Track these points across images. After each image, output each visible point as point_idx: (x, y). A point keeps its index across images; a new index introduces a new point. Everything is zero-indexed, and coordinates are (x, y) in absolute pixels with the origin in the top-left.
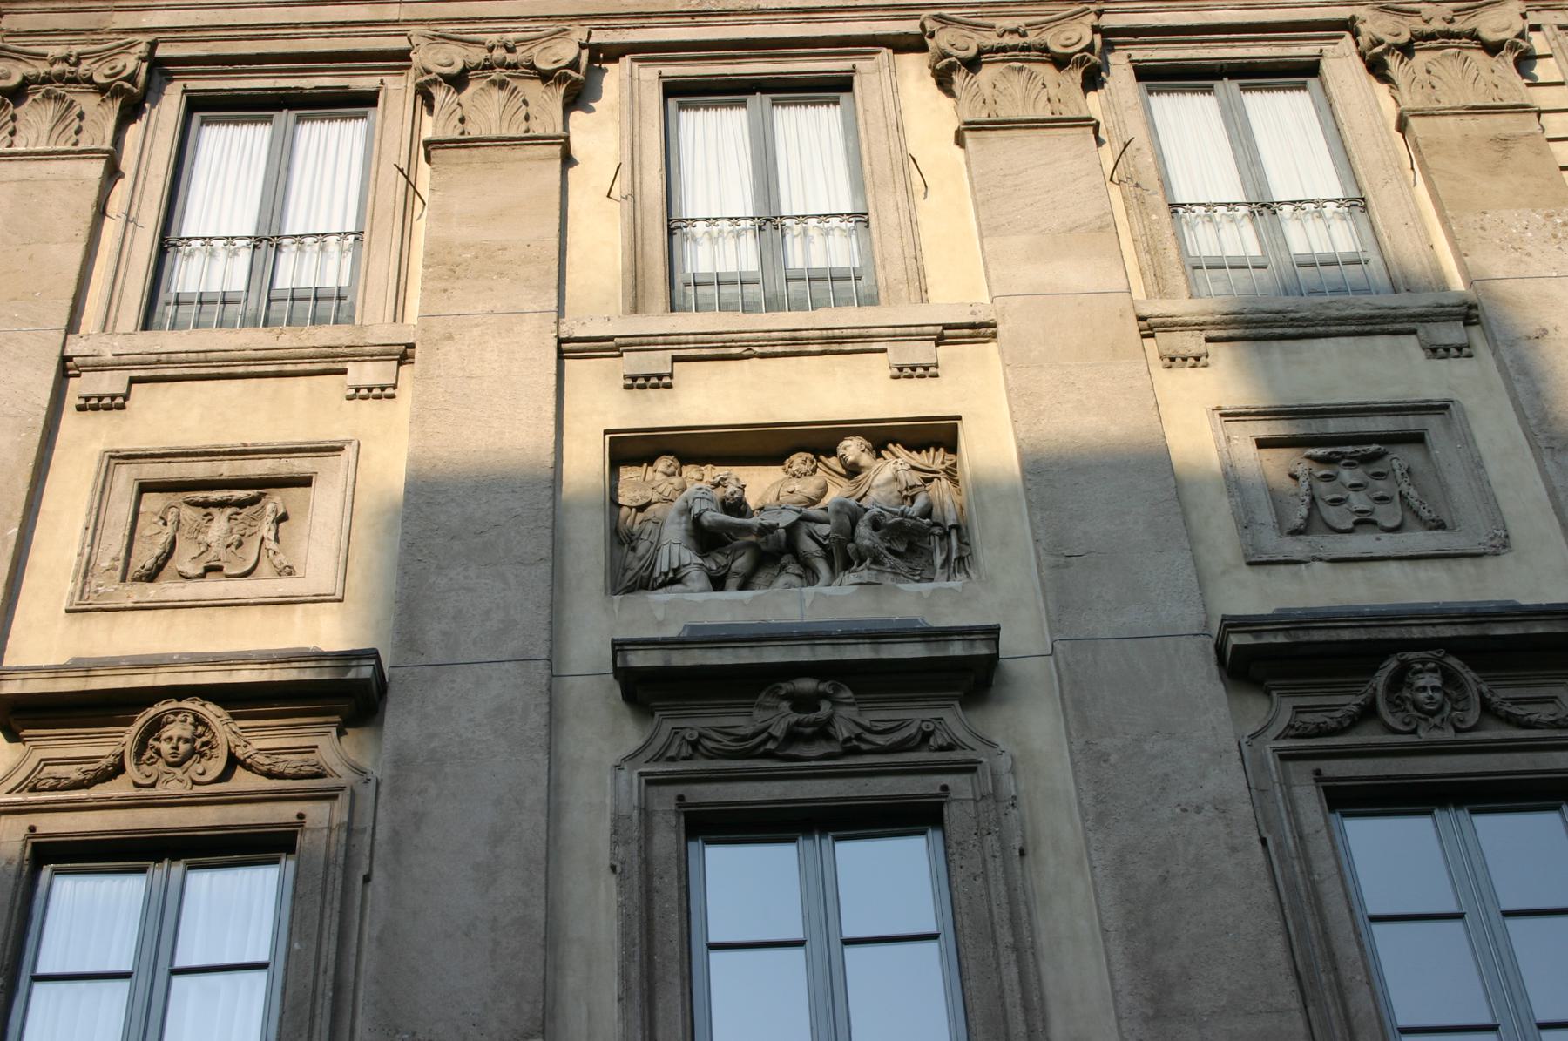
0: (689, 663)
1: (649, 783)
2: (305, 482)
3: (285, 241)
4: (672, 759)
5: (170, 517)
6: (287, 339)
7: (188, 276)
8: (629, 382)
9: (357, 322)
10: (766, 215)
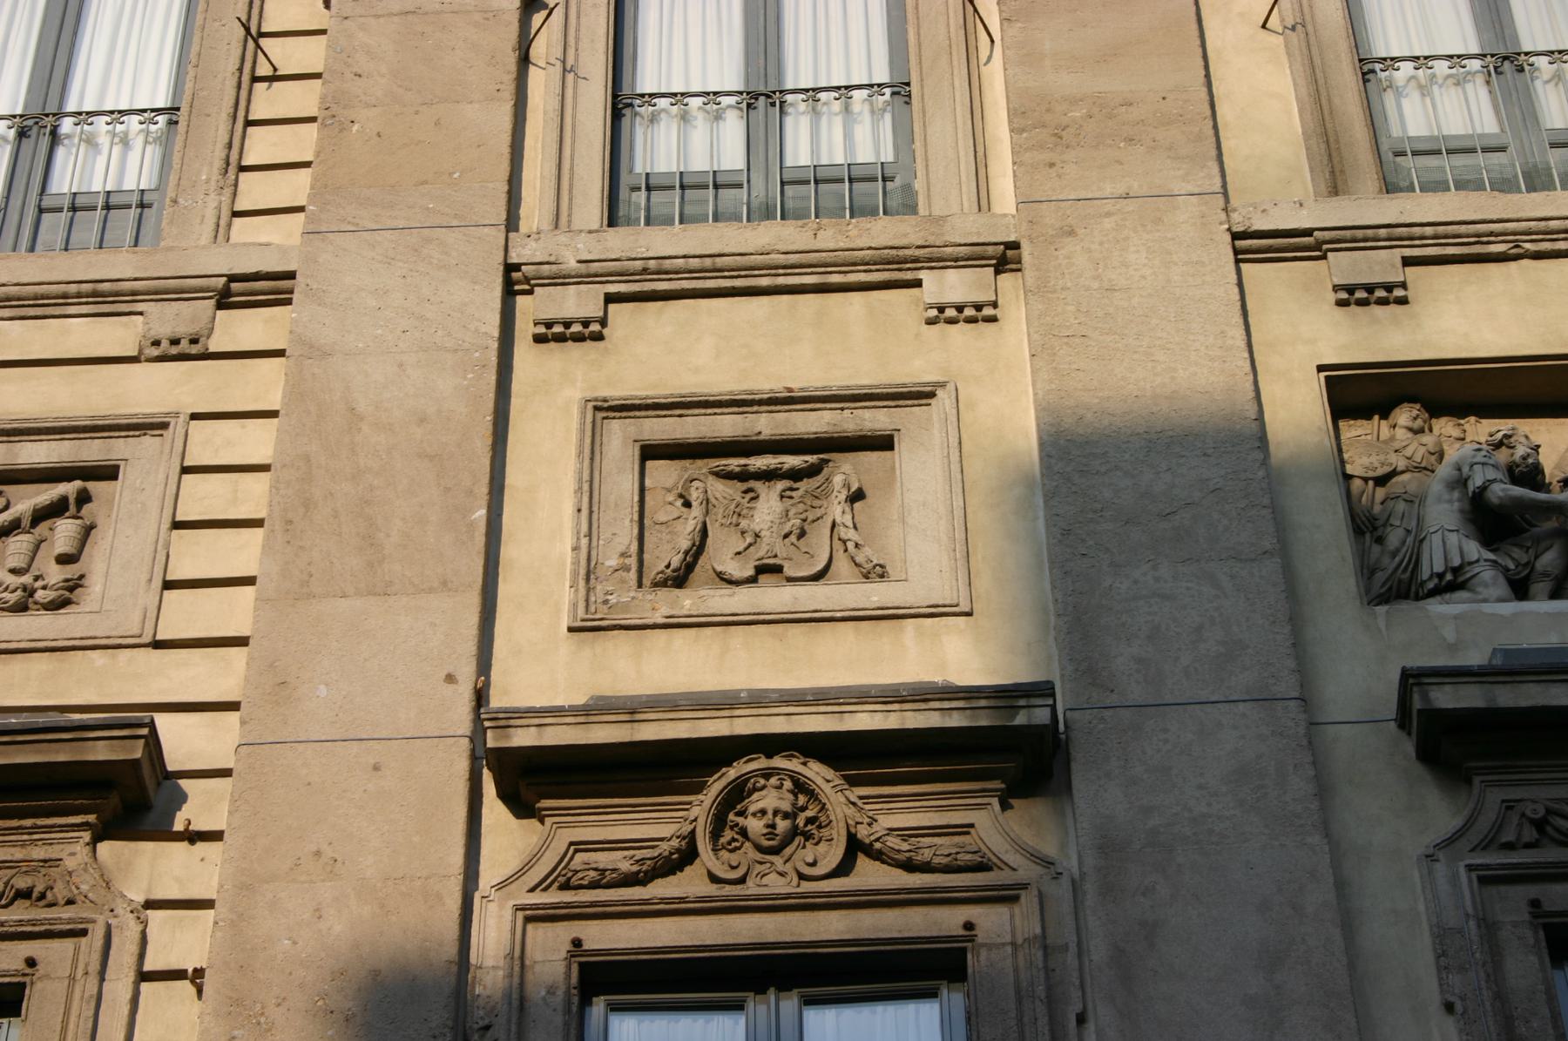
0: (1523, 703)
1: (1483, 881)
2: (884, 443)
3: (789, 98)
4: (1509, 846)
5: (695, 495)
6: (831, 237)
7: (661, 148)
8: (1344, 295)
9: (922, 210)
10: (1502, 51)
